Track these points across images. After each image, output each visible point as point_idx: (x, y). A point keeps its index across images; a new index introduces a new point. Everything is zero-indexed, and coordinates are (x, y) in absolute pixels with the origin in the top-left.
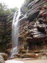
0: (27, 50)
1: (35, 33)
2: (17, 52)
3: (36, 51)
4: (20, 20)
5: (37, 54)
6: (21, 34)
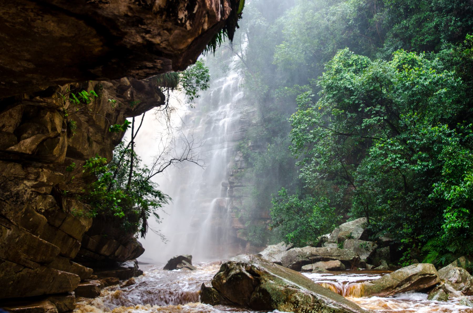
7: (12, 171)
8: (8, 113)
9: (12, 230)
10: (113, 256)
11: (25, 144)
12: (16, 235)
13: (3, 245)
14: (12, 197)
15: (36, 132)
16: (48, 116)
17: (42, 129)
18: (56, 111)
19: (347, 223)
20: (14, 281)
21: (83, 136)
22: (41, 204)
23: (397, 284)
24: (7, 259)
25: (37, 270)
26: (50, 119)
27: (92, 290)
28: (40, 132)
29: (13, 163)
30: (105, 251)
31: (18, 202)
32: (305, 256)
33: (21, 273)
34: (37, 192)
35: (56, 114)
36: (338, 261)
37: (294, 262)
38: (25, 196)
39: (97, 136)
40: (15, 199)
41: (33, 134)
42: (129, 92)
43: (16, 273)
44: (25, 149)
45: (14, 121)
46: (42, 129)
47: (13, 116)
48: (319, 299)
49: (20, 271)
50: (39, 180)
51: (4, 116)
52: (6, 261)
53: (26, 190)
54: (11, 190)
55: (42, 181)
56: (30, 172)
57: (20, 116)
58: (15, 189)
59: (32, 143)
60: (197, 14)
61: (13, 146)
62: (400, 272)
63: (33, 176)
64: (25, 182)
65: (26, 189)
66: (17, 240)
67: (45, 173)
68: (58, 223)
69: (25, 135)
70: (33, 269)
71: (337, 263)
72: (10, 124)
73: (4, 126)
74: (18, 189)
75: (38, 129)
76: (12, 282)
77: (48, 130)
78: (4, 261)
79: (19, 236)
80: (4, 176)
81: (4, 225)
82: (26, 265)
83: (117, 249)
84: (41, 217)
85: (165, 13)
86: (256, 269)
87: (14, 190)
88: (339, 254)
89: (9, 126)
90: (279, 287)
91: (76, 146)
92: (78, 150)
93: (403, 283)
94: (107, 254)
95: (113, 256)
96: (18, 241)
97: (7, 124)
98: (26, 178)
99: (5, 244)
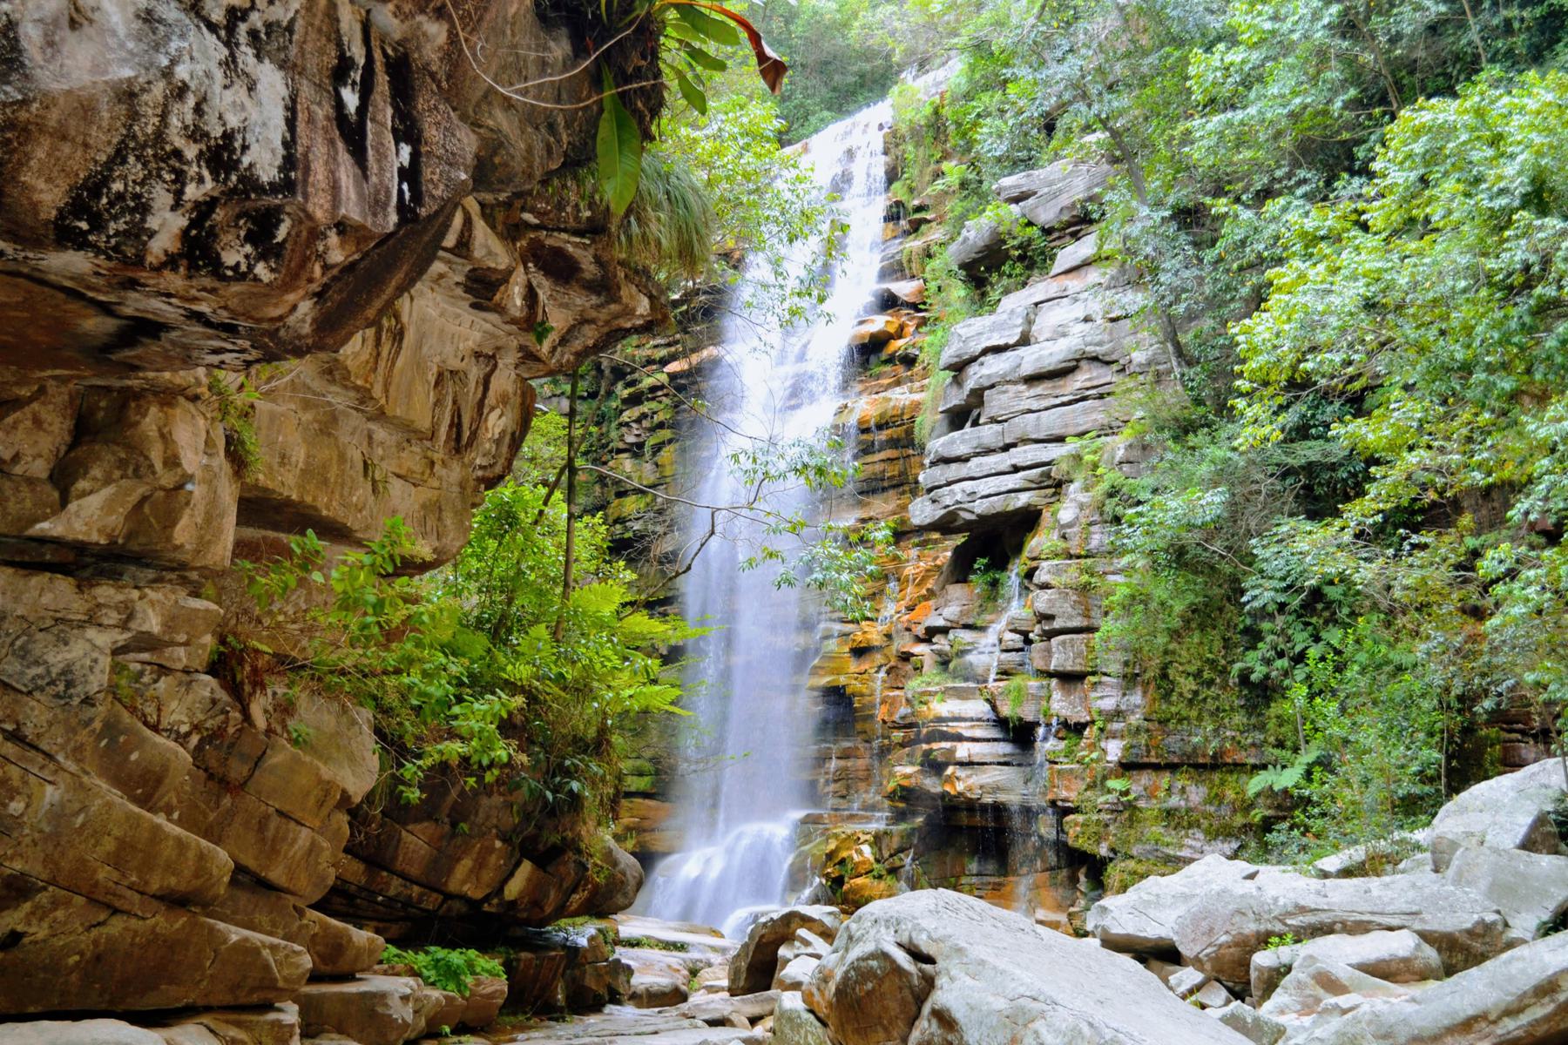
1: (963, 751)
6: (860, 652)
7: (44, 600)
8: (29, 416)
9: (62, 786)
10: (495, 901)
11: (83, 514)
12: (77, 806)
13: (37, 835)
14: (52, 683)
15: (117, 474)
16: (151, 420)
17: (134, 464)
18: (181, 400)
19: (1492, 782)
20: (81, 954)
21: (342, 458)
22: (174, 705)
23: (1503, 1006)
24: (53, 882)
25: (157, 924)
26: (160, 430)
27: (380, 1010)
28: (130, 471)
29: (48, 575)
30: (464, 882)
31: (70, 697)
32: (1270, 911)
33: (104, 930)
34: (160, 666)
35: (178, 411)
36: (1404, 931)
37: (1224, 938)
38: (92, 678)
39: (404, 455)
40: (61, 687)
41: (108, 481)
42: (517, 289)
43: (88, 929)
44: (84, 528)
45: (50, 439)
46: (134, 464)
47: (45, 425)
48: (1108, 1037)
49: (99, 924)
50: (133, 625)
51: (15, 426)
52: (51, 888)
53: (95, 661)
54: (46, 662)
55: (144, 628)
56: (101, 600)
57: (69, 424)
58: (59, 657)
59: (108, 507)
60: (289, 246)
61: (45, 518)
62: (1518, 959)
63: (113, 617)
64: (91, 633)
65: (95, 655)
66: (80, 820)
67: (152, 603)
68: (237, 770)
69: (82, 484)
70: (143, 919)
71: (1401, 944)
72: (35, 451)
73: (16, 458)
74: (69, 656)
75: (122, 464)
76: (77, 958)
77: (151, 466)
78: (45, 889)
79: (83, 809)
80: (23, 617)
81: (35, 771)
82: (118, 904)
83: (511, 874)
84: (169, 749)
85: (184, 262)
86: (924, 936)
87: (57, 658)
88: (1415, 908)
89: (34, 458)
90: (991, 999)
91: (314, 499)
92: (325, 513)
93: (1526, 1001)
94: (473, 891)
95: (495, 901)
96: (83, 825)
97: (27, 449)
98: (92, 620)
99: (41, 831)
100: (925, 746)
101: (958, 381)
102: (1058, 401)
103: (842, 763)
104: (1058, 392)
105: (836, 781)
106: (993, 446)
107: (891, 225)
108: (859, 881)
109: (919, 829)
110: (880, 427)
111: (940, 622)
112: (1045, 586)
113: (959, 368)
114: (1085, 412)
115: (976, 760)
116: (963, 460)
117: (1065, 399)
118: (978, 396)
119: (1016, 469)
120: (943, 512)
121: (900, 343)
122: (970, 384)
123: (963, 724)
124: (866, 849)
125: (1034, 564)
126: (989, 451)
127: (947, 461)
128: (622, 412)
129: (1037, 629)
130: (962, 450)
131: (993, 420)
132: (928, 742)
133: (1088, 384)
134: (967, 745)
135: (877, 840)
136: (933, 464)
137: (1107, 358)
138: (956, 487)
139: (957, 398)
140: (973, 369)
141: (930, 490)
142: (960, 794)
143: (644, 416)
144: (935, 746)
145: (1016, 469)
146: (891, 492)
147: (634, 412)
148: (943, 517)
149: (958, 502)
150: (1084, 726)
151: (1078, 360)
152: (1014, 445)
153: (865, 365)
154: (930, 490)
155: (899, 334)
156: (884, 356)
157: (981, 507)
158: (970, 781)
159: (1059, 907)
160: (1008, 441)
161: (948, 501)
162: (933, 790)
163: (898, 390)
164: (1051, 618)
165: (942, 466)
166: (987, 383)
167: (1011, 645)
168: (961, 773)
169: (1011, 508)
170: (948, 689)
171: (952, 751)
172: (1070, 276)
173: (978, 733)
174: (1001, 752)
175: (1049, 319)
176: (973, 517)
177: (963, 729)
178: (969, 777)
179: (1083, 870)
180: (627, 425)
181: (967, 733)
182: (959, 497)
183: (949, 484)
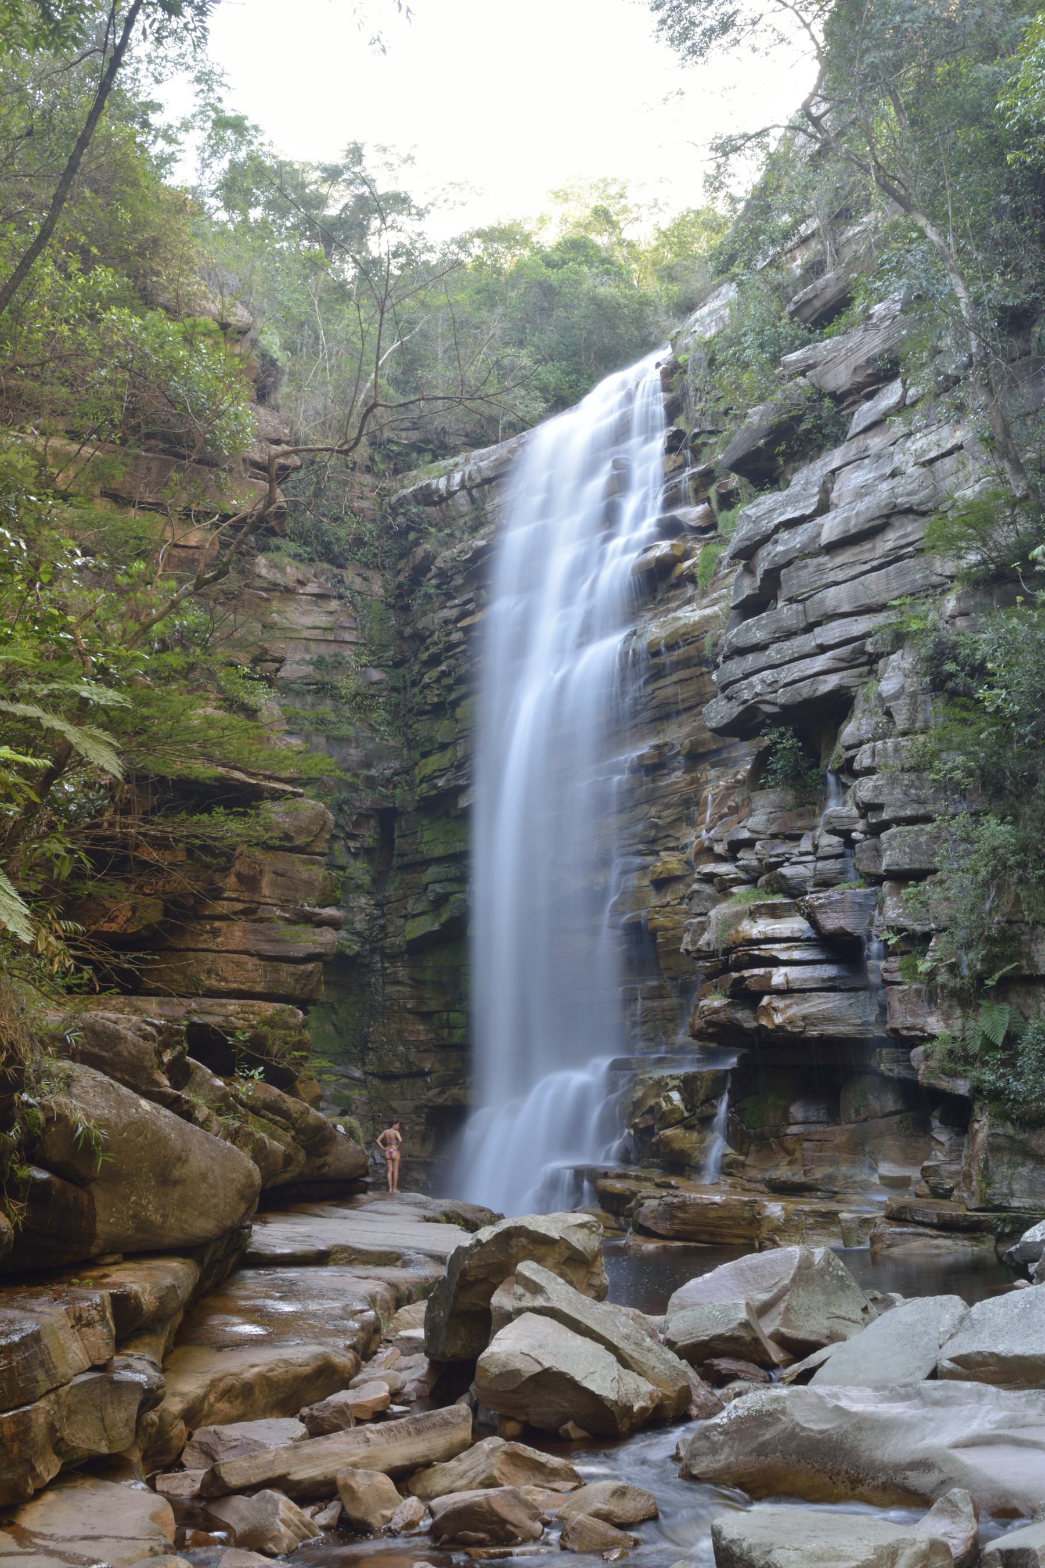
0: (717, 1148)
1: (779, 976)
2: (605, 1134)
3: (783, 1172)
4: (655, 630)
5: (775, 1209)
6: (661, 884)
100: (735, 975)
101: (749, 570)
102: (867, 567)
103: (649, 1003)
104: (866, 556)
105: (644, 1023)
106: (794, 628)
107: (673, 456)
108: (669, 1132)
109: (733, 1071)
110: (671, 647)
111: (746, 835)
112: (870, 771)
113: (747, 554)
114: (901, 574)
115: (796, 986)
116: (760, 648)
117: (875, 563)
118: (772, 579)
119: (823, 649)
120: (741, 708)
121: (687, 563)
122: (762, 566)
123: (777, 946)
124: (676, 1096)
125: (851, 753)
126: (790, 634)
127: (742, 652)
128: (423, 674)
129: (860, 825)
130: (759, 636)
131: (791, 600)
132: (738, 970)
133: (903, 542)
134: (783, 970)
135: (687, 1085)
136: (727, 658)
137: (923, 508)
138: (755, 679)
139: (749, 587)
140: (763, 552)
141: (724, 688)
142: (780, 1027)
143: (443, 674)
144: (746, 973)
145: (823, 649)
146: (684, 716)
147: (435, 673)
148: (741, 714)
149: (757, 695)
150: (927, 937)
151: (888, 516)
152: (818, 624)
153: (654, 590)
154: (724, 688)
155: (687, 555)
156: (673, 579)
157: (782, 697)
158: (790, 1012)
159: (910, 1159)
160: (811, 620)
161: (746, 695)
162: (746, 1025)
163: (688, 608)
164: (879, 807)
165: (737, 659)
166: (783, 561)
167: (828, 851)
168: (779, 1003)
169: (819, 693)
170: (759, 907)
171: (768, 977)
172: (870, 434)
173: (796, 955)
174: (825, 975)
175: (853, 479)
176: (776, 709)
177: (778, 951)
178: (788, 1007)
179: (48, 763)
180: (428, 686)
181: (784, 956)
182: (759, 689)
183: (746, 676)
